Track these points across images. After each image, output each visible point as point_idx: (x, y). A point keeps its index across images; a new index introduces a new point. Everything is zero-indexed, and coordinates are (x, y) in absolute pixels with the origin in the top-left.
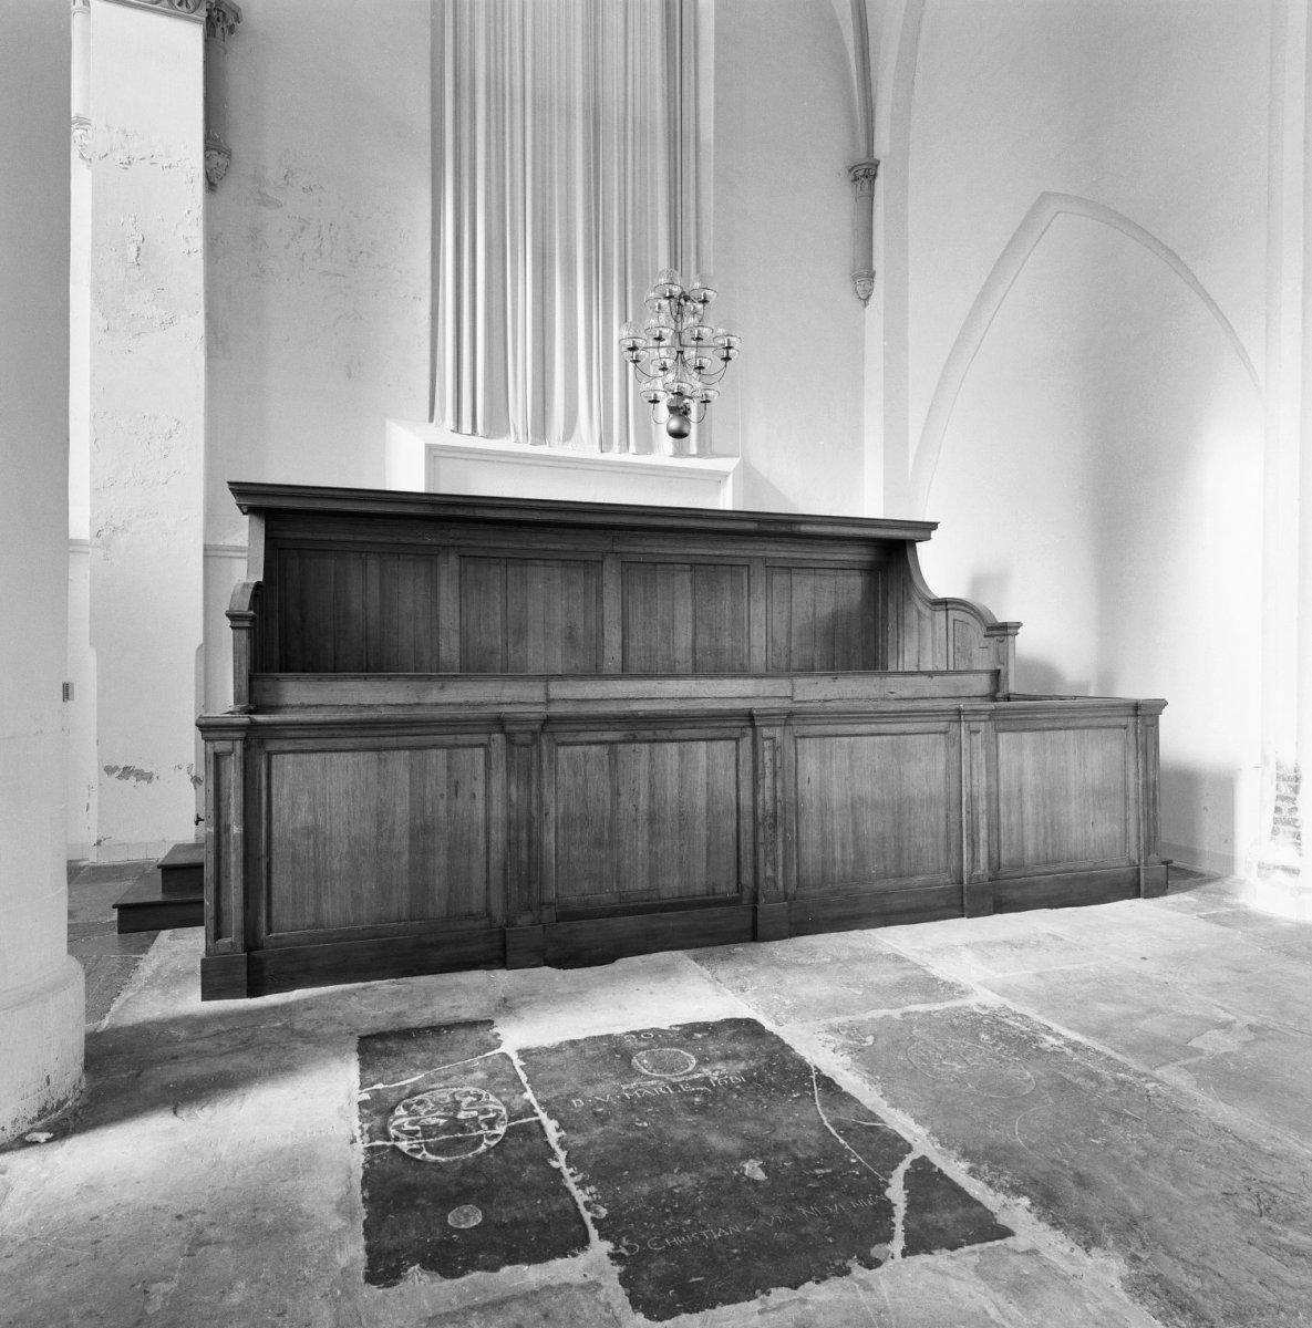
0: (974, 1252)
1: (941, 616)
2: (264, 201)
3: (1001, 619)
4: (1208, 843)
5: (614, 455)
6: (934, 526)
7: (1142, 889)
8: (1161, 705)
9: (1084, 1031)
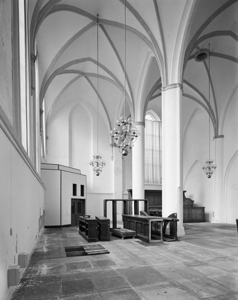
0: (216, 221)
1: (187, 200)
2: (125, 162)
3: (192, 200)
4: (210, 219)
5: (155, 184)
6: (186, 191)
7: (156, 210)
8: (205, 207)
9: (51, 266)
